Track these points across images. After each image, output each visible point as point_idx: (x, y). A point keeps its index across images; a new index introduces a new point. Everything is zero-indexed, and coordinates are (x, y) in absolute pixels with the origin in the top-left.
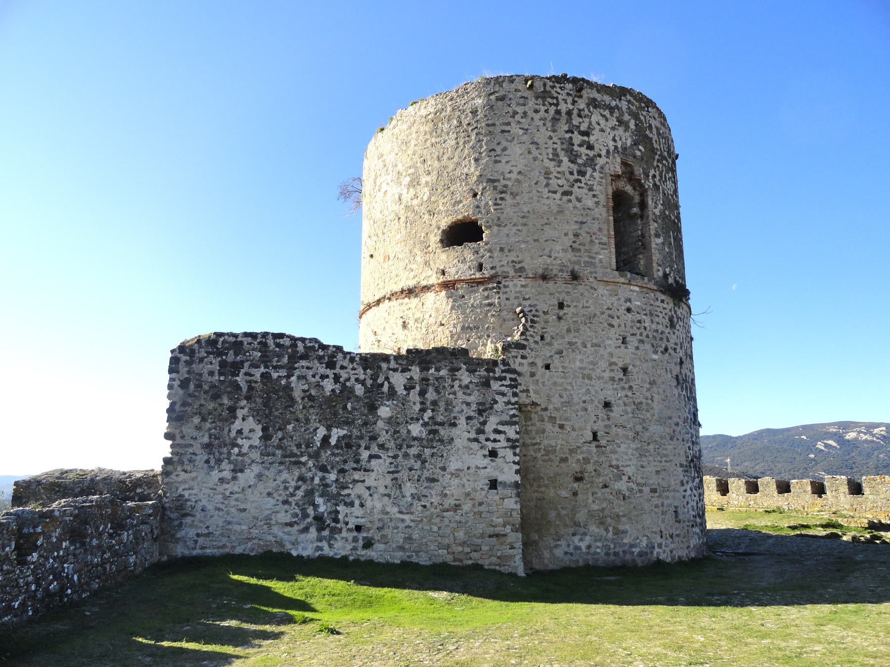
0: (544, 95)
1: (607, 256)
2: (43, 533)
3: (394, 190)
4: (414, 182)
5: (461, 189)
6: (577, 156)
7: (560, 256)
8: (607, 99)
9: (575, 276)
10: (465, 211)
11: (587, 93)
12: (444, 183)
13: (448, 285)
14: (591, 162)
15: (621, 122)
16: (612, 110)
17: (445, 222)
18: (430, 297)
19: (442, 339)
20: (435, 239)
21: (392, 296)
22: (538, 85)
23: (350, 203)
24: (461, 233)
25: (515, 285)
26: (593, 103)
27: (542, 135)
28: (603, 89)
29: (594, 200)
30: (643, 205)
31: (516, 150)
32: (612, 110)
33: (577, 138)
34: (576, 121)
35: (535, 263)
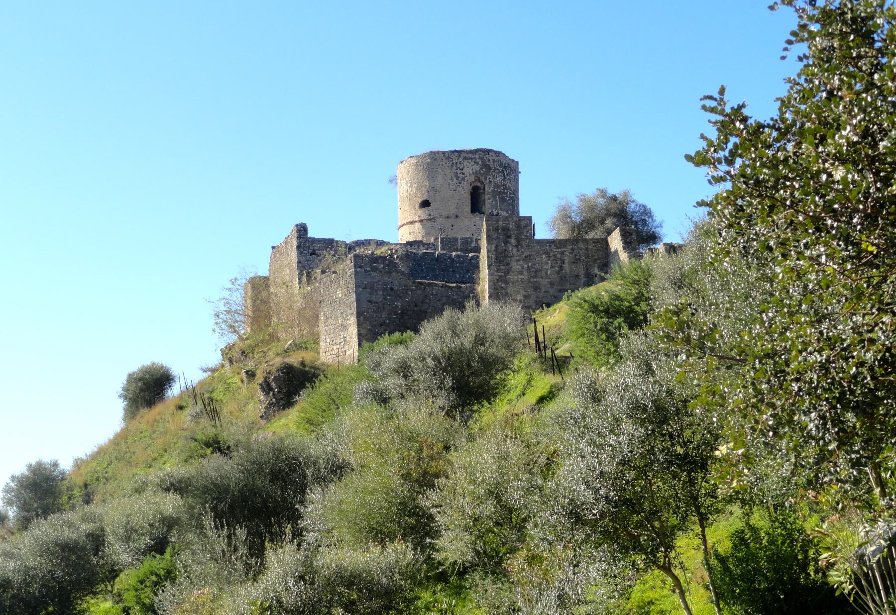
0: (449, 158)
1: (468, 209)
2: (850, 48)
3: (406, 187)
4: (411, 186)
5: (424, 189)
6: (459, 177)
7: (453, 211)
8: (470, 155)
9: (457, 217)
10: (425, 197)
11: (463, 155)
12: (419, 188)
13: (421, 221)
14: (463, 179)
15: (475, 163)
16: (472, 159)
17: (420, 200)
18: (417, 224)
19: (419, 238)
20: (417, 206)
21: (406, 224)
22: (447, 155)
23: (393, 184)
24: (425, 204)
25: (439, 221)
26: (465, 158)
27: (448, 171)
28: (471, 152)
29: (465, 192)
30: (484, 189)
31: (440, 177)
32: (472, 159)
33: (459, 171)
34: (459, 165)
35: (445, 214)
